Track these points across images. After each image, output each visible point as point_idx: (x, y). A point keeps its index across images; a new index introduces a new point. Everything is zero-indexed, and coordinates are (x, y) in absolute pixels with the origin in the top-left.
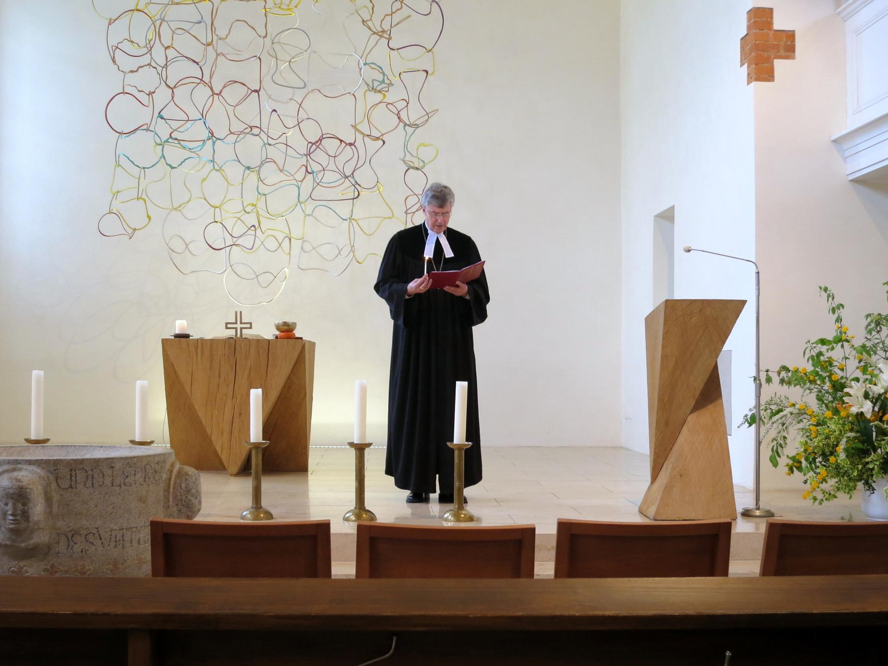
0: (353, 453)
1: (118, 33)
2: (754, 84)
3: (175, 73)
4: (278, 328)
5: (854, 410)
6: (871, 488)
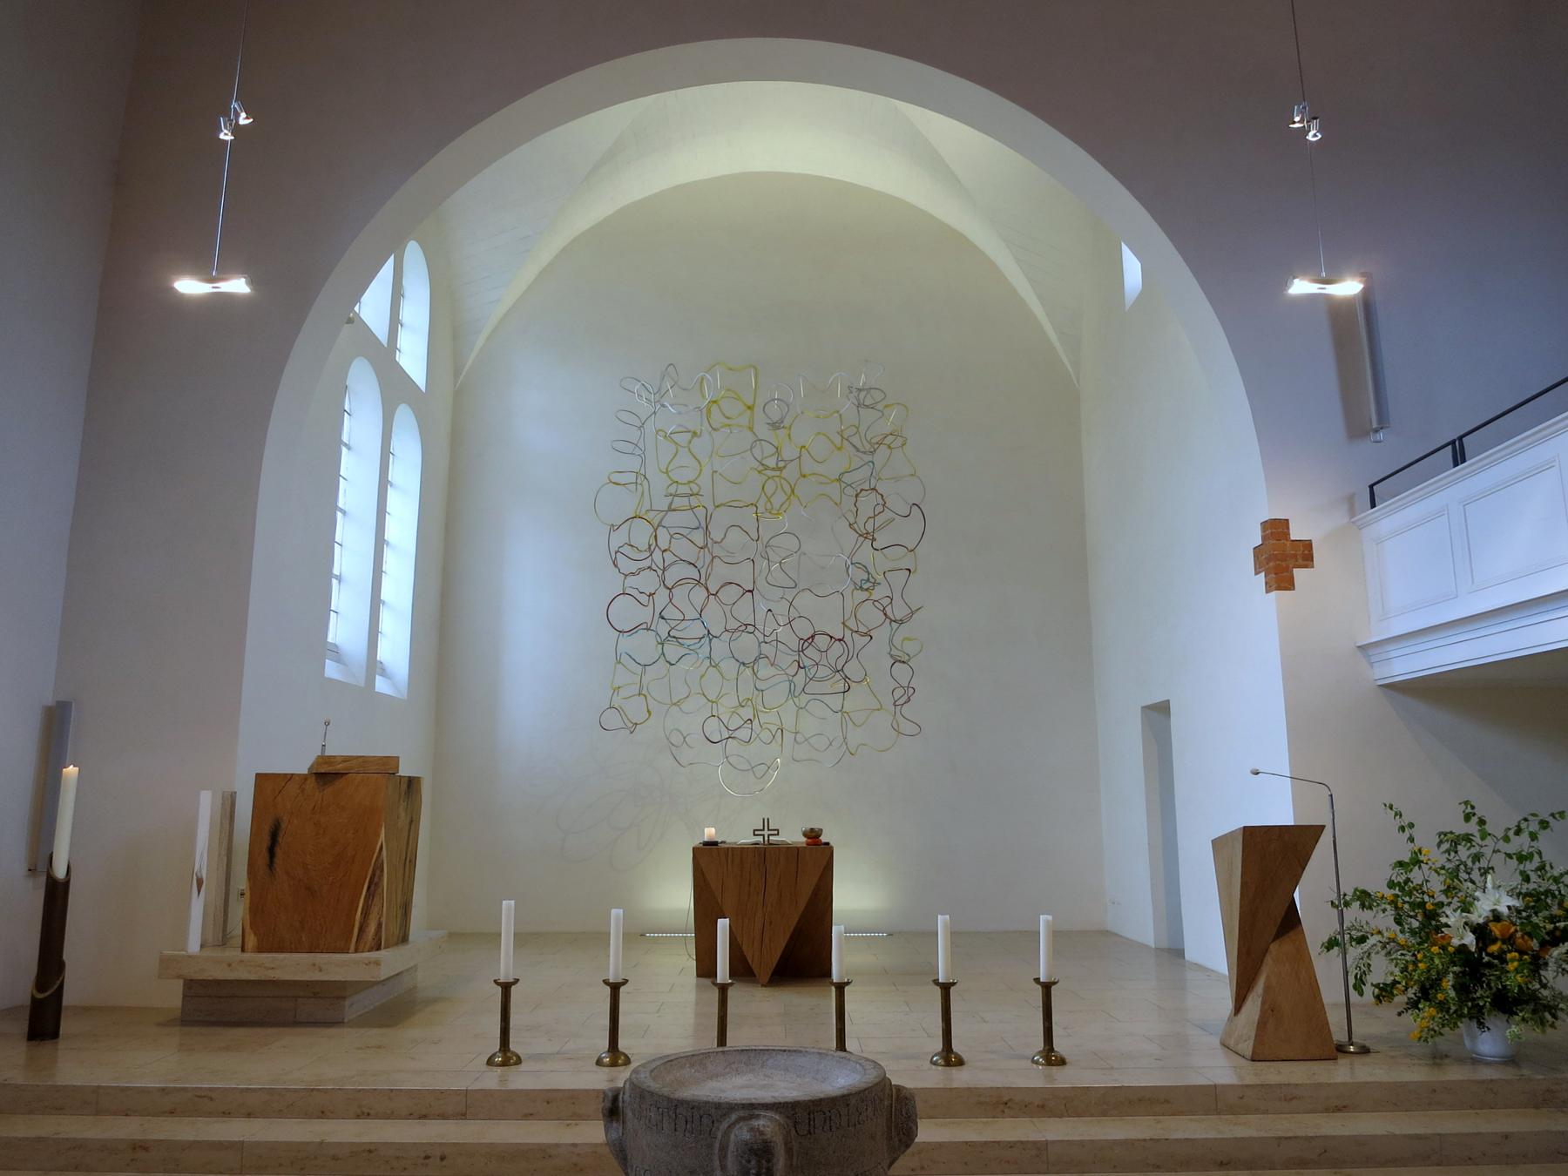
0: (938, 991)
1: (619, 539)
2: (1274, 594)
3: (671, 577)
4: (805, 834)
5: (1456, 942)
6: (1481, 1025)
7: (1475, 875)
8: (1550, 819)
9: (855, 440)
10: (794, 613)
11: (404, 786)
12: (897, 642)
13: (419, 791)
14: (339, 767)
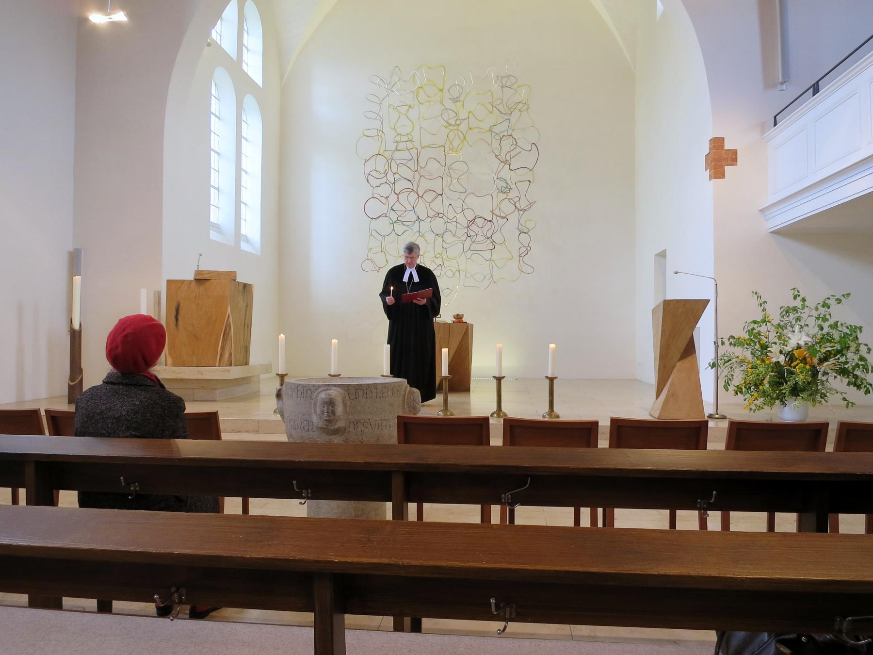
1: (369, 167)
3: (399, 187)
5: (774, 360)
6: (783, 403)
7: (797, 328)
8: (842, 298)
9: (501, 108)
10: (465, 206)
11: (241, 288)
12: (522, 222)
13: (251, 292)
14: (206, 277)
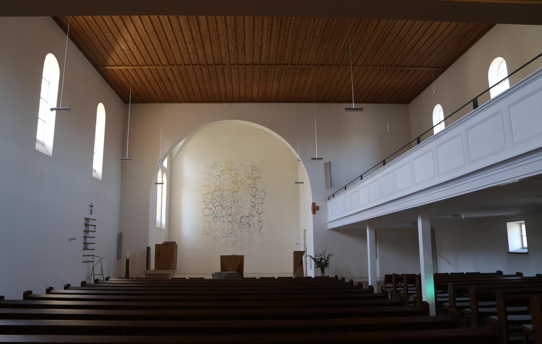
9: (252, 177)
